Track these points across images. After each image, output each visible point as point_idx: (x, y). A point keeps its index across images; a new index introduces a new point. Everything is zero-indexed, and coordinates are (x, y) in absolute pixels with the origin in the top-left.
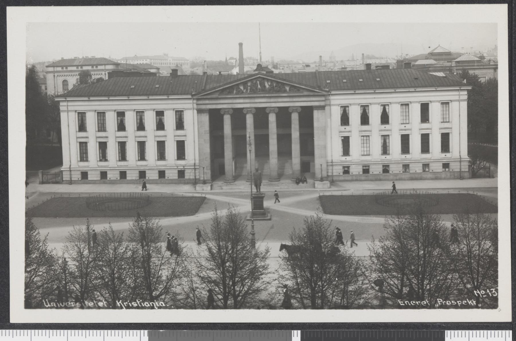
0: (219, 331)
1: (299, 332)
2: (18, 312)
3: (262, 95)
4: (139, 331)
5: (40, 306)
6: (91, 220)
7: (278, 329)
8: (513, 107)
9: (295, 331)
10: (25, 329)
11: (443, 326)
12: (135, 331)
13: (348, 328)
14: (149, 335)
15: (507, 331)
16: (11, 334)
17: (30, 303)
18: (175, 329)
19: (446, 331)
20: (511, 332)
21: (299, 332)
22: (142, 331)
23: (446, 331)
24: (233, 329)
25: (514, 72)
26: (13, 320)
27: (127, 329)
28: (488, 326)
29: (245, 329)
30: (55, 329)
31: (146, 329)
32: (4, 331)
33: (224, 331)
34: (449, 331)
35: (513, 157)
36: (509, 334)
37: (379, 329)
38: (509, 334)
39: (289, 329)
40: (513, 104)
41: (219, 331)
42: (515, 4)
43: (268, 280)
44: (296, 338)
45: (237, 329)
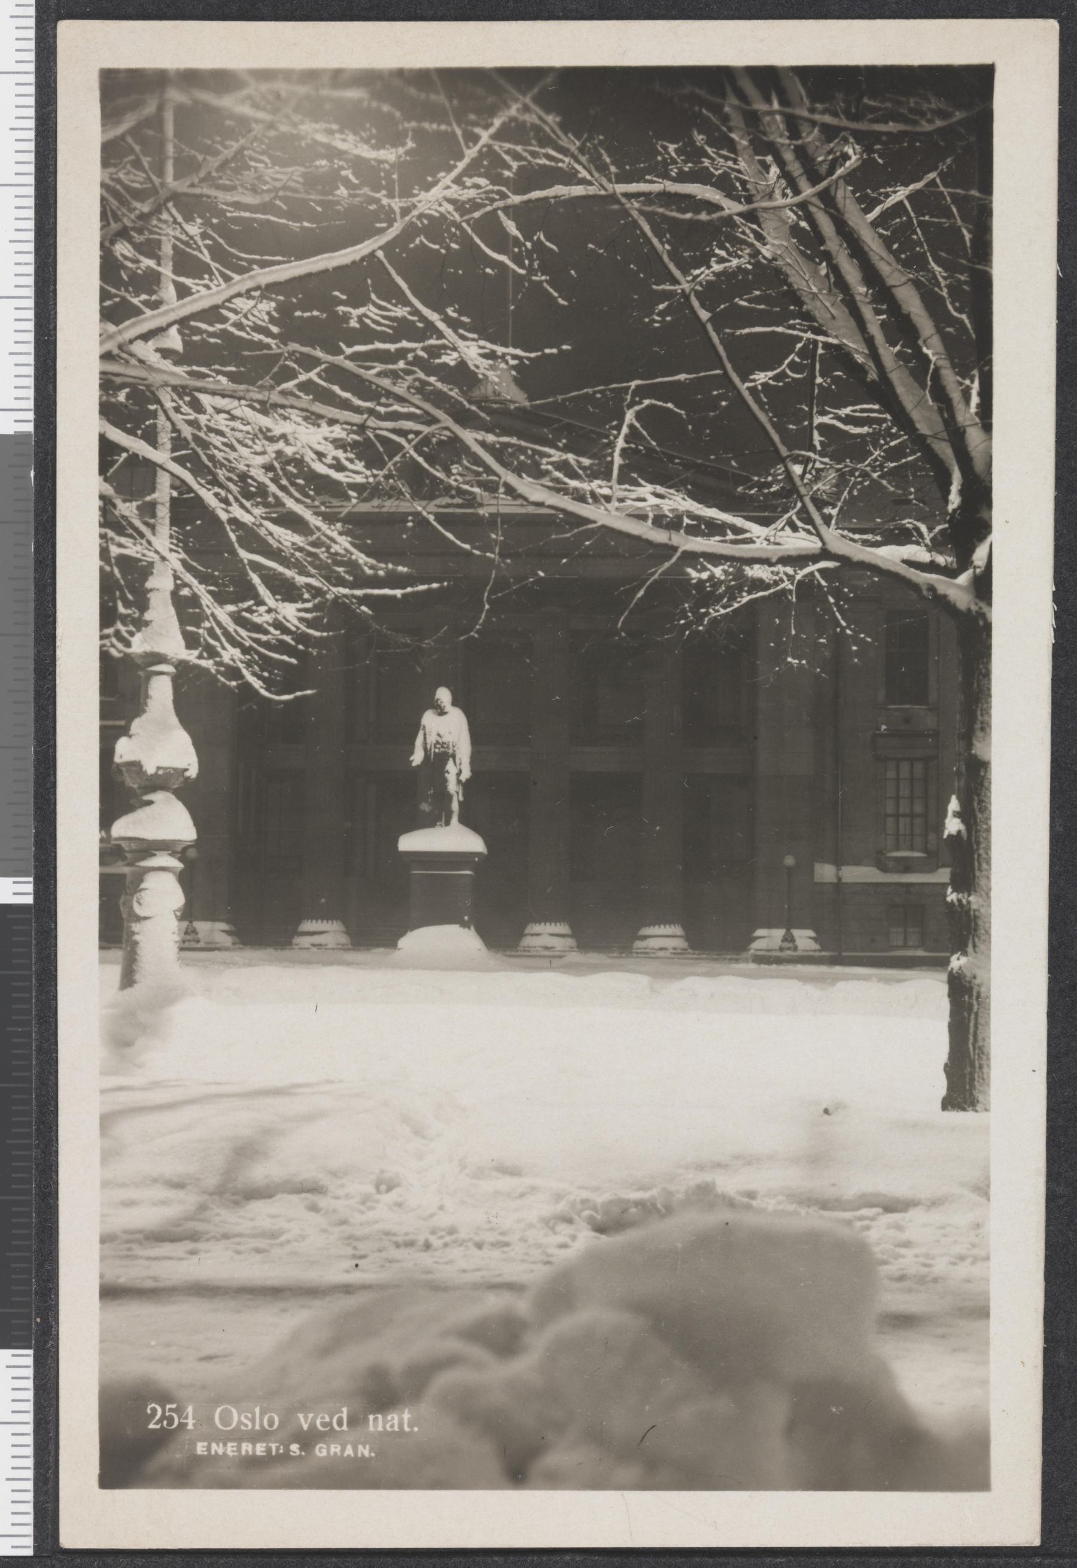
0: (31, 574)
1: (29, 900)
2: (92, 46)
3: (971, 1038)
4: (30, 404)
5: (110, 113)
6: (672, 532)
7: (36, 835)
8: (722, 1560)
9: (30, 888)
10: (37, 55)
11: (46, 1342)
12: (31, 393)
13: (39, 1049)
14: (18, 438)
15: (30, 1541)
16: (21, 11)
17: (119, 88)
18: (37, 515)
19: (31, 1352)
20: (30, 1552)
21: (29, 900)
22: (31, 416)
23: (31, 1352)
24: (38, 695)
25: (830, 1560)
26: (68, 30)
27: (36, 369)
28: (46, 1482)
29: (36, 732)
30: (36, 303)
31: (36, 427)
32: (32, 11)
33: (31, 666)
34: (30, 1361)
35: (568, 1558)
36: (23, 1546)
37: (38, 1146)
38: (23, 1546)
39: (36, 867)
40: (732, 1560)
41: (30, 652)
42: (1040, 1564)
43: (267, 1224)
44: (9, 890)
45: (38, 808)
